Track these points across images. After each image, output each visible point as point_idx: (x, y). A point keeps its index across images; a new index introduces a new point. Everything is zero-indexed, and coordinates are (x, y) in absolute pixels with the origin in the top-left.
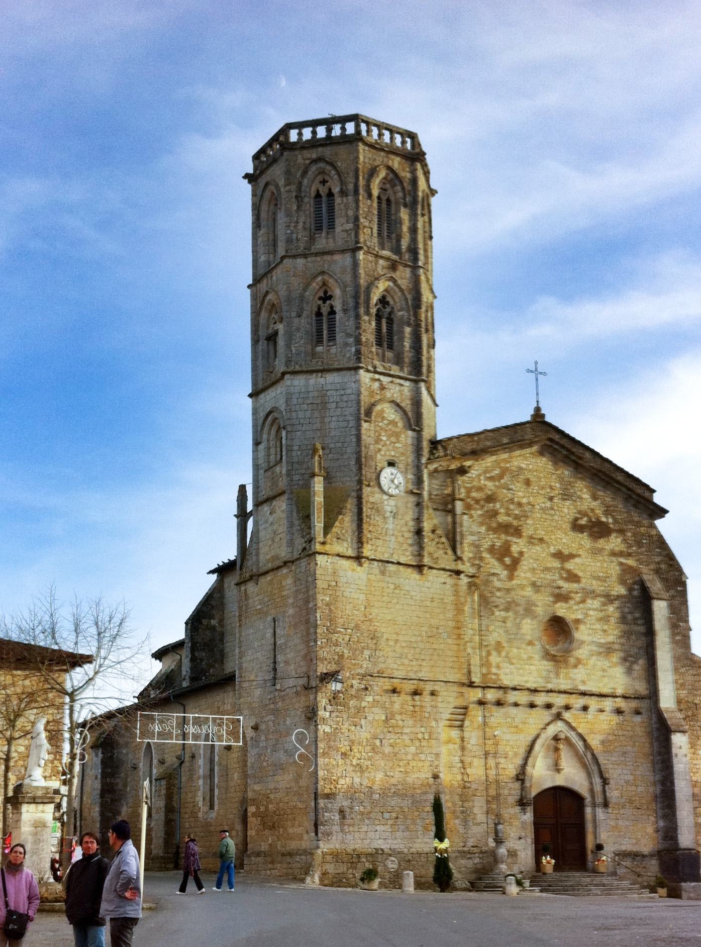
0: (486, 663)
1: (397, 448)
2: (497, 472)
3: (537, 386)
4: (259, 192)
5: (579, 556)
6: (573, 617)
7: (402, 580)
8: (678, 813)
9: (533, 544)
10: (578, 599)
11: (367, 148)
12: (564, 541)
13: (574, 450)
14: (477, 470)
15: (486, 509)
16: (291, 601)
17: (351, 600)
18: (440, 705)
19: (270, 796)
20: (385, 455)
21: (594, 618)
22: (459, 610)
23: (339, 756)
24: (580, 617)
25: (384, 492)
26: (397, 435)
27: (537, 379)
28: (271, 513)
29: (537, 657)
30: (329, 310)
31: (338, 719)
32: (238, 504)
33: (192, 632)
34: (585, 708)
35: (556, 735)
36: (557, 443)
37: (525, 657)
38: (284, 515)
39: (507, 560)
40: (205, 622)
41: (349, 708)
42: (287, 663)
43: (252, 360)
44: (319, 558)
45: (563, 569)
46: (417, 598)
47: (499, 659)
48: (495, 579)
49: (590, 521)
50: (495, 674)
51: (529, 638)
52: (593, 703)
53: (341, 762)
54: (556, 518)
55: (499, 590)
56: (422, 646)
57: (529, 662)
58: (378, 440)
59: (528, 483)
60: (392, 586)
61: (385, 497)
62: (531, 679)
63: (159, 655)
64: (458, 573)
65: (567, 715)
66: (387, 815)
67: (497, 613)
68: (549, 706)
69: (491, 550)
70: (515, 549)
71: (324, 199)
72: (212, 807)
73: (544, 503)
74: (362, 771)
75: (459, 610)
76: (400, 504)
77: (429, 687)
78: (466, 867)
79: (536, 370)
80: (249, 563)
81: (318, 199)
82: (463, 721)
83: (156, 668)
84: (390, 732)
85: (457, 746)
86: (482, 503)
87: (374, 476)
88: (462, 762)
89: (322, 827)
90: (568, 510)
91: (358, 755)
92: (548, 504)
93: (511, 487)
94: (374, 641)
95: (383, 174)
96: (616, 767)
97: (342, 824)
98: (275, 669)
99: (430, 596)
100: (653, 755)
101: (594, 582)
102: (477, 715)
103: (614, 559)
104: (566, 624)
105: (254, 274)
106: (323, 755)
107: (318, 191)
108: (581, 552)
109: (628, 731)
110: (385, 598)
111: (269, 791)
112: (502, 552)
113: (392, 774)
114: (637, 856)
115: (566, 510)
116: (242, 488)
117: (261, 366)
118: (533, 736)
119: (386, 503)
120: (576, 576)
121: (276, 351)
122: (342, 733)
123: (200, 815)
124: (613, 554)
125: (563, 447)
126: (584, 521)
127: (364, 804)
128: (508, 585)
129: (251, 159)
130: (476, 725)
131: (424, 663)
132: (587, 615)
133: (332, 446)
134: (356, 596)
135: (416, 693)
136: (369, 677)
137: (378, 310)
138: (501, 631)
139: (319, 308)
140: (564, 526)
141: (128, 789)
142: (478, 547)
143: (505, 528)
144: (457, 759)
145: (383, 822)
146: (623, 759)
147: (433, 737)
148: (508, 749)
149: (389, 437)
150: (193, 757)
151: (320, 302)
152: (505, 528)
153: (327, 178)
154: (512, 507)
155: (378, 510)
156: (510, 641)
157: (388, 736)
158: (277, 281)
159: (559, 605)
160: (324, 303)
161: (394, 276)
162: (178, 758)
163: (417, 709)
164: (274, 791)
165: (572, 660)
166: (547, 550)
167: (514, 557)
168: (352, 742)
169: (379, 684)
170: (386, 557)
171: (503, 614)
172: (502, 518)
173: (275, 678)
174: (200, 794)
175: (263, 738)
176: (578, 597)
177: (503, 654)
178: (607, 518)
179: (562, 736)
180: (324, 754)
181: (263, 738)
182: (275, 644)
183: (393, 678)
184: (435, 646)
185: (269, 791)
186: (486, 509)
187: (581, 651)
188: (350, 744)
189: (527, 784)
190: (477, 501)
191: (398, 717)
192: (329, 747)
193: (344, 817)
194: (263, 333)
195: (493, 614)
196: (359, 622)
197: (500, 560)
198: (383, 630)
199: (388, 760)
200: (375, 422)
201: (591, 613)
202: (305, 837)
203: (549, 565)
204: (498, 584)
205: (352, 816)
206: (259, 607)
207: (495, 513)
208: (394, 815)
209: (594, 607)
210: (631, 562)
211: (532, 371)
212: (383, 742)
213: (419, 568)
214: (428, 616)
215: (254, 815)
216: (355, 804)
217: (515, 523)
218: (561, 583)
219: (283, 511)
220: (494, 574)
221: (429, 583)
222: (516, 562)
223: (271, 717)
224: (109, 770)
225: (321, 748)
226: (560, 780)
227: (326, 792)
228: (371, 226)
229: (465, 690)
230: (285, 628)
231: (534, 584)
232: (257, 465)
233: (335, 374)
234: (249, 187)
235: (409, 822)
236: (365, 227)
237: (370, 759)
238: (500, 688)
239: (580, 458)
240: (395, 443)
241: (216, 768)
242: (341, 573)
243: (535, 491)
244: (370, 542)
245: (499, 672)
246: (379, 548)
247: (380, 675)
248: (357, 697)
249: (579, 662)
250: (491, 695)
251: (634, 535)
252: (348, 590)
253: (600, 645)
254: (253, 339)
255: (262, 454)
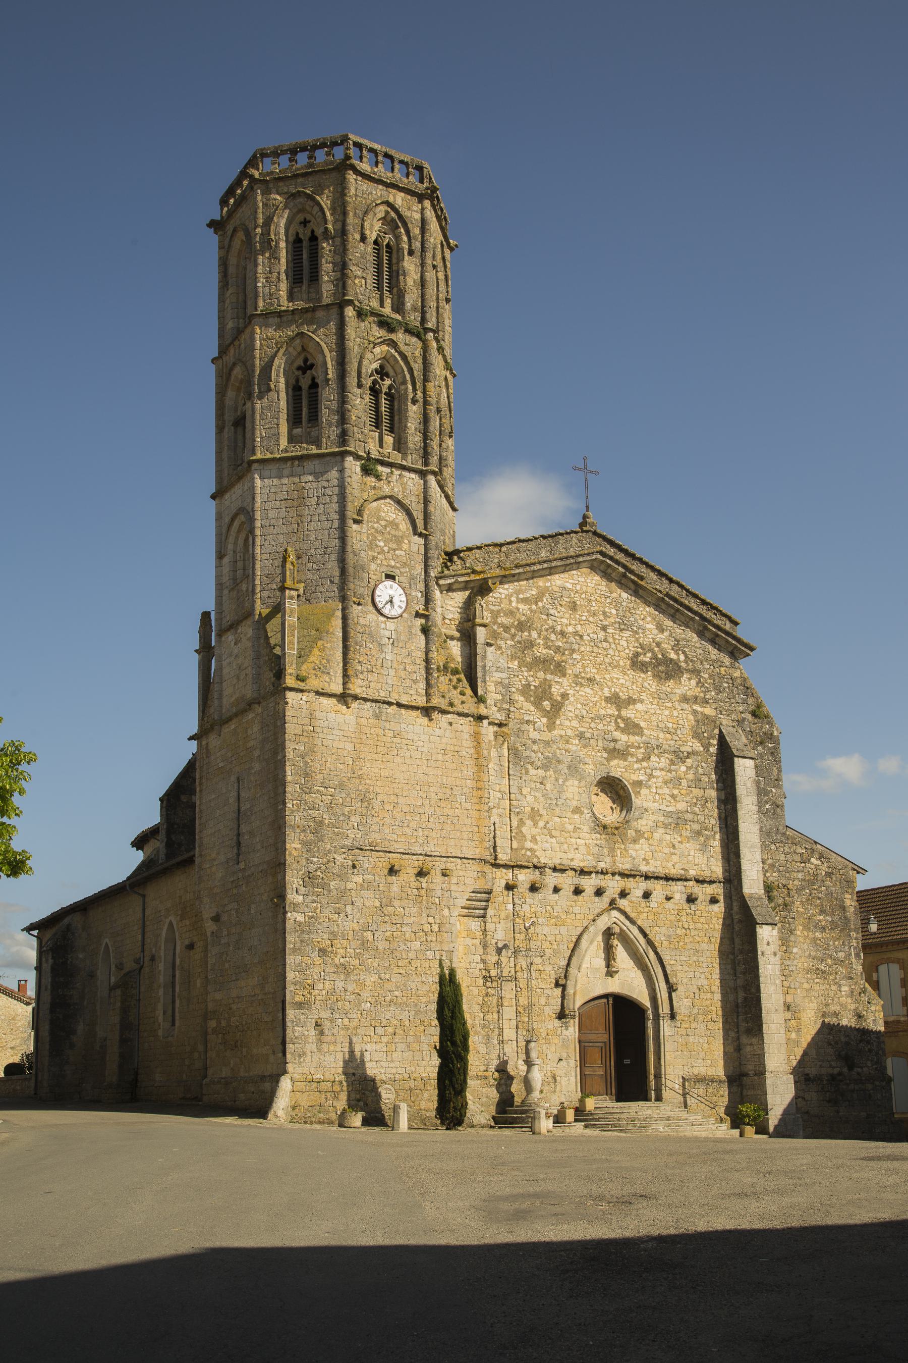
0: (516, 834)
1: (398, 556)
2: (534, 593)
3: (587, 488)
4: (226, 243)
5: (642, 701)
6: (634, 777)
7: (403, 725)
8: (764, 1026)
9: (581, 685)
10: (640, 756)
11: (360, 178)
12: (622, 681)
13: (633, 567)
14: (507, 589)
15: (517, 638)
16: (257, 753)
17: (334, 751)
18: (453, 888)
19: (232, 1006)
20: (381, 565)
21: (660, 780)
22: (480, 766)
23: (316, 953)
24: (643, 778)
25: (379, 611)
26: (399, 540)
27: (586, 480)
28: (236, 644)
29: (586, 828)
30: (310, 382)
31: (315, 905)
32: (200, 637)
33: (167, 810)
34: (647, 895)
35: (609, 929)
36: (611, 558)
37: (570, 828)
38: (249, 644)
39: (546, 704)
40: (184, 798)
41: (329, 891)
42: (251, 833)
43: (216, 453)
44: (290, 695)
45: (619, 716)
46: (425, 749)
47: (535, 831)
48: (531, 727)
49: (655, 656)
50: (530, 850)
51: (575, 803)
52: (658, 889)
53: (318, 961)
54: (611, 652)
55: (534, 742)
56: (431, 811)
57: (576, 835)
58: (371, 546)
59: (574, 607)
60: (391, 734)
61: (382, 619)
62: (578, 856)
63: (139, 843)
64: (480, 718)
65: (623, 903)
66: (380, 1031)
67: (532, 771)
68: (599, 892)
69: (525, 690)
70: (555, 690)
71: (305, 244)
72: (173, 1024)
73: (594, 633)
74: (347, 975)
75: (480, 766)
76: (401, 628)
77: (440, 864)
78: (487, 1097)
79: (586, 467)
80: (212, 710)
81: (298, 245)
82: (485, 909)
83: (139, 857)
84: (385, 922)
85: (477, 942)
86: (513, 630)
87: (367, 592)
88: (484, 962)
89: (291, 1046)
90: (626, 644)
91: (341, 951)
92: (602, 635)
93: (552, 612)
94: (365, 805)
95: (381, 210)
96: (686, 968)
97: (320, 1042)
98: (239, 844)
99: (443, 747)
100: (733, 954)
101: (661, 735)
102: (502, 904)
103: (686, 706)
104: (624, 788)
105: (220, 346)
106: (293, 952)
107: (297, 234)
108: (643, 696)
109: (702, 923)
110: (379, 749)
111: (231, 1001)
112: (540, 695)
113: (387, 977)
114: (713, 1081)
115: (624, 643)
116: (206, 616)
117: (226, 459)
118: (580, 930)
119: (383, 626)
120: (637, 726)
121: (244, 436)
122: (320, 923)
123: (160, 1033)
124: (685, 699)
125: (617, 562)
126: (647, 658)
127: (349, 1016)
128: (547, 736)
129: (218, 202)
130: (503, 916)
131: (433, 834)
132: (651, 776)
133: (313, 552)
134: (341, 745)
135: (421, 874)
136: (357, 850)
137: (375, 382)
138: (539, 795)
139: (297, 381)
140: (621, 663)
141: (85, 1003)
142: (507, 687)
143: (542, 663)
144: (478, 958)
145: (376, 1038)
146: (695, 958)
147: (444, 929)
148: (546, 945)
149: (386, 542)
150: (153, 959)
151: (300, 373)
152: (542, 663)
153: (309, 217)
154: (553, 637)
155: (370, 634)
156: (549, 808)
157: (384, 927)
158: (245, 348)
159: (614, 762)
160: (304, 373)
161: (395, 339)
162: (137, 961)
163: (423, 892)
164: (236, 1000)
165: (631, 833)
166: (600, 693)
167: (556, 701)
168: (334, 935)
169: (371, 859)
170: (383, 695)
171: (540, 772)
172: (541, 651)
173: (238, 855)
174: (160, 1007)
175: (225, 933)
176: (640, 753)
177: (541, 824)
178: (678, 654)
179: (617, 930)
180: (295, 950)
181: (225, 933)
182: (239, 810)
183: (390, 852)
184: (446, 811)
185: (231, 1001)
186: (517, 638)
187: (643, 822)
188: (331, 937)
189: (570, 990)
190: (506, 629)
191: (397, 903)
192: (302, 941)
193: (322, 1033)
194: (229, 417)
195: (527, 772)
196: (345, 779)
197: (537, 704)
198: (378, 790)
199: (383, 959)
200: (368, 522)
201: (657, 773)
202: (272, 1058)
203: (602, 712)
204: (534, 735)
205: (335, 1031)
206: (221, 765)
207: (531, 645)
208: (390, 1030)
209: (662, 765)
210: (709, 711)
211: (580, 469)
212: (376, 936)
213: (427, 711)
214: (439, 772)
215: (215, 1031)
216: (336, 1016)
217: (557, 657)
218: (617, 735)
219: (249, 639)
220: (528, 722)
221: (442, 731)
222: (557, 707)
223: (234, 905)
224: (62, 979)
225: (290, 942)
226: (614, 986)
227: (297, 999)
228: (364, 275)
229: (488, 868)
230: (249, 789)
231: (581, 736)
232: (221, 584)
233: (316, 462)
234: (216, 238)
235: (410, 1039)
236: (356, 277)
237: (358, 956)
238: (535, 867)
239: (642, 578)
240: (395, 550)
241: (178, 973)
242: (320, 715)
243: (584, 618)
244: (361, 676)
245: (535, 847)
246: (372, 684)
247: (373, 848)
248: (340, 876)
249: (640, 834)
250: (524, 877)
251: (711, 676)
252: (329, 737)
253: (668, 814)
254: (217, 426)
255: (226, 570)
